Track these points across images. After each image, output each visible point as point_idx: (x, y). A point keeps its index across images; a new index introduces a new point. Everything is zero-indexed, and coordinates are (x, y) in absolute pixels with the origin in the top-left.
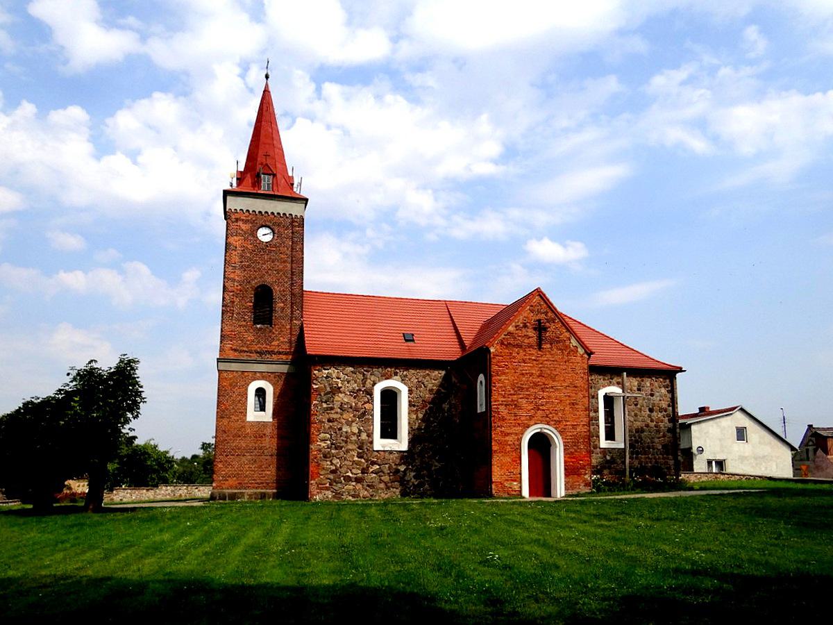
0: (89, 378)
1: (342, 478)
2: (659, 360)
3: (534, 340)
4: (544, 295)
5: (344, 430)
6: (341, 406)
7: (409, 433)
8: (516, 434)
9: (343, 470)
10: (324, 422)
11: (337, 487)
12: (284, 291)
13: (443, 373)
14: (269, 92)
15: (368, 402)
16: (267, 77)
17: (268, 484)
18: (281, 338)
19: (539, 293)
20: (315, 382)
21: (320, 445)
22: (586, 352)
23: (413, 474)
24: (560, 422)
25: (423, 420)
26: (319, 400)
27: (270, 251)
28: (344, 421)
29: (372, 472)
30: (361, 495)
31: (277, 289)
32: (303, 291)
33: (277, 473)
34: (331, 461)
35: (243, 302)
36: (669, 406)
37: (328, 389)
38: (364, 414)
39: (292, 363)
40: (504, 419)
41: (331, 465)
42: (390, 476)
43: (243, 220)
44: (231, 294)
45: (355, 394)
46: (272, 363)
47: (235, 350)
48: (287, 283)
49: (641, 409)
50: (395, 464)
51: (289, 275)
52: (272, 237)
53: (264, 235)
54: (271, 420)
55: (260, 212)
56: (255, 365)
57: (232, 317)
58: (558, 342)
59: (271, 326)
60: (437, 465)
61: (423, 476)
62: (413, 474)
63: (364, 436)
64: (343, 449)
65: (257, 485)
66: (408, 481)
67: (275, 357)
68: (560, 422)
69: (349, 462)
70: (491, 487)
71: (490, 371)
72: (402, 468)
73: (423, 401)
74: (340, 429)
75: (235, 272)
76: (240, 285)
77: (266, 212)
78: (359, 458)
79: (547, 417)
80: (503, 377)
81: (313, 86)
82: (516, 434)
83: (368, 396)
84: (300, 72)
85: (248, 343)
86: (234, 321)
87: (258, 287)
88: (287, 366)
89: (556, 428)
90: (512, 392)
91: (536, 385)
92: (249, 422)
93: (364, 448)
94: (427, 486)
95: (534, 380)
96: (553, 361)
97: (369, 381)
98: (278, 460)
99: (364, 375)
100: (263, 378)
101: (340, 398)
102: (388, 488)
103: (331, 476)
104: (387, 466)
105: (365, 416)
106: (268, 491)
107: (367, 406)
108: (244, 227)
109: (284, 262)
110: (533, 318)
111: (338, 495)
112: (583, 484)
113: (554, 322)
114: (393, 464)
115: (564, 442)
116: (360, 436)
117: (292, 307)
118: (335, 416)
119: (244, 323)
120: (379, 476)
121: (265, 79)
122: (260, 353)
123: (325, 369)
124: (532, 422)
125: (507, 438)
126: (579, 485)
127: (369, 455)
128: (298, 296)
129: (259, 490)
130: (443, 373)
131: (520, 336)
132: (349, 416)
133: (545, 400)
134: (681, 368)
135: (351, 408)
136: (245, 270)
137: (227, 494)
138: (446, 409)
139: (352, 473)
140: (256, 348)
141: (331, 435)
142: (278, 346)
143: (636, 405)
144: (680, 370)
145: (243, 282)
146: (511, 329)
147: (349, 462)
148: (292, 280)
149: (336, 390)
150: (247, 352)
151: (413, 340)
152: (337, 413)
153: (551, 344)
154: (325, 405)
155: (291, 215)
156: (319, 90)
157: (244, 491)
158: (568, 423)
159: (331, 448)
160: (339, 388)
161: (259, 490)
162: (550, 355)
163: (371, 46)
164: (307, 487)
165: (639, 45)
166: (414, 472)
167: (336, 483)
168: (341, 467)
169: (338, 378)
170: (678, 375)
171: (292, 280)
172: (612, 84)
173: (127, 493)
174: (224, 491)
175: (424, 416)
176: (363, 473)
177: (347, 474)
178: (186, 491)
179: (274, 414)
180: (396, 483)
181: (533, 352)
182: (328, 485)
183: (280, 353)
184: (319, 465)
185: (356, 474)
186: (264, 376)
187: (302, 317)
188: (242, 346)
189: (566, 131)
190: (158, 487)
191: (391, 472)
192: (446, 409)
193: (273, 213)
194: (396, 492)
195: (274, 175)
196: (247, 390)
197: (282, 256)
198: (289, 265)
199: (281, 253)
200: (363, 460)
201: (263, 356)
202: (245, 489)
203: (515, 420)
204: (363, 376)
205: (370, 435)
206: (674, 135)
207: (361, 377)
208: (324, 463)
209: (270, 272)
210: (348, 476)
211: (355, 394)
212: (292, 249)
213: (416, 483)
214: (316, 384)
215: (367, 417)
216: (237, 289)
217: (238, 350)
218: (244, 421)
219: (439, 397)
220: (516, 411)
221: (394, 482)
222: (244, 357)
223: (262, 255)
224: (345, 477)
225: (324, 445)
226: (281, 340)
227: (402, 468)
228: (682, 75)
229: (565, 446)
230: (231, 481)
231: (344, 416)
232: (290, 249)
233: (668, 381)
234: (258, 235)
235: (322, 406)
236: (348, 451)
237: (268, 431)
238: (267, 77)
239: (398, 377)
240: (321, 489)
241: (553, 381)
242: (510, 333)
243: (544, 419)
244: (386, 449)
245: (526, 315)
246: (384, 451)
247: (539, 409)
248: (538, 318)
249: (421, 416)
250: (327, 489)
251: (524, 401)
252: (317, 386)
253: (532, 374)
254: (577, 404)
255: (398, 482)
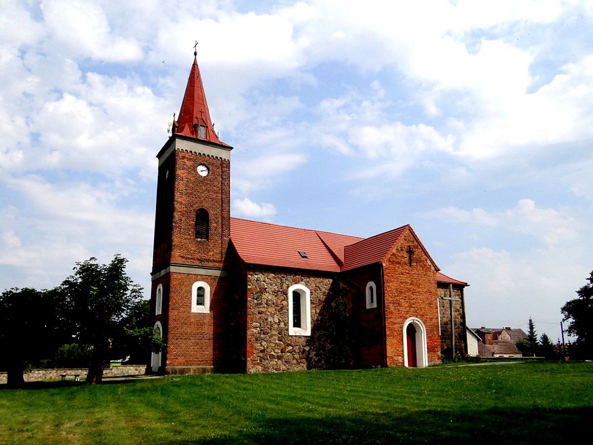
0: (88, 271)
1: (268, 356)
2: (452, 278)
3: (407, 260)
4: (412, 230)
5: (269, 320)
6: (267, 302)
7: (311, 323)
8: (399, 323)
9: (269, 350)
10: (255, 314)
11: (265, 363)
12: (216, 214)
13: (331, 280)
14: (197, 65)
15: (284, 300)
16: (195, 54)
17: (207, 361)
18: (215, 250)
19: (408, 228)
20: (249, 283)
21: (253, 331)
22: (435, 269)
23: (314, 353)
24: (423, 315)
25: (319, 314)
26: (252, 297)
27: (207, 184)
28: (269, 313)
29: (288, 352)
30: (281, 369)
31: (211, 212)
32: (230, 218)
33: (213, 353)
34: (261, 343)
35: (188, 220)
36: (460, 308)
37: (258, 289)
38: (282, 308)
39: (224, 269)
40: (392, 313)
41: (261, 346)
42: (299, 354)
43: (187, 158)
44: (179, 213)
45: (275, 293)
46: (210, 268)
47: (183, 257)
48: (219, 208)
49: (446, 309)
50: (303, 346)
51: (220, 203)
52: (207, 173)
53: (202, 171)
54: (209, 312)
55: (199, 154)
56: (198, 269)
57: (180, 231)
58: (421, 262)
59: (208, 240)
60: (329, 346)
61: (320, 355)
62: (314, 353)
63: (282, 325)
64: (269, 334)
65: (199, 363)
66: (311, 358)
67: (211, 264)
68: (423, 315)
69: (272, 345)
70: (386, 360)
71: (383, 279)
72: (307, 349)
73: (319, 300)
74: (266, 319)
75: (182, 197)
76: (186, 207)
77: (204, 154)
78: (279, 341)
79: (416, 312)
80: (391, 284)
81: (80, 74)
82: (399, 323)
83: (285, 296)
84: (70, 61)
85: (192, 252)
86: (182, 235)
87: (199, 210)
88: (220, 271)
89: (422, 320)
90: (396, 294)
91: (409, 290)
92: (193, 313)
93: (283, 333)
94: (323, 362)
95: (408, 286)
96: (418, 274)
97: (285, 284)
98: (214, 343)
99: (281, 280)
100: (203, 280)
101: (266, 296)
102: (299, 363)
103: (261, 355)
104: (298, 347)
105: (282, 309)
106: (207, 367)
107: (284, 303)
108: (188, 163)
109: (217, 193)
110: (406, 244)
111: (265, 368)
112: (437, 358)
113: (418, 248)
114: (301, 346)
115: (426, 330)
116: (279, 325)
117: (222, 227)
118: (263, 310)
119: (189, 237)
120: (293, 355)
121: (194, 56)
122: (200, 260)
123: (255, 275)
124: (408, 316)
125: (394, 326)
126: (435, 359)
127: (286, 339)
128: (226, 219)
129: (201, 366)
130: (331, 280)
131: (399, 256)
132: (272, 310)
133: (414, 301)
134: (467, 284)
135: (273, 303)
136: (189, 197)
137: (177, 370)
138: (334, 307)
139: (274, 352)
140: (198, 256)
141: (260, 323)
142: (213, 256)
143: (443, 307)
144: (466, 285)
145: (188, 205)
146: (394, 251)
147: (272, 345)
148: (222, 207)
149: (263, 290)
150: (191, 259)
151: (306, 257)
152: (264, 307)
153: (416, 263)
154: (256, 301)
155: (221, 158)
156: (84, 78)
157: (190, 367)
158: (428, 317)
159: (260, 333)
160: (266, 289)
161: (201, 366)
162: (416, 270)
163: (127, 51)
164: (245, 362)
165: (312, 80)
166: (315, 351)
167: (265, 360)
168: (267, 348)
169: (264, 282)
170: (465, 289)
171: (222, 207)
172: (294, 103)
173: (4, 377)
174: (175, 367)
175: (320, 311)
176: (282, 352)
177: (271, 353)
178: (55, 374)
179: (211, 308)
180: (303, 359)
181: (407, 267)
182: (258, 361)
183: (215, 261)
184: (252, 346)
185: (278, 353)
186: (203, 278)
187: (229, 235)
188: (187, 254)
189: (265, 128)
190: (31, 371)
191: (300, 352)
192: (334, 307)
193: (208, 156)
194: (304, 366)
195: (207, 127)
196: (191, 288)
197: (215, 188)
198: (220, 195)
199: (214, 186)
200: (282, 343)
201: (202, 263)
202: (190, 365)
203: (398, 314)
204: (281, 281)
205: (286, 324)
206: (329, 141)
207: (279, 281)
208: (256, 345)
209: (206, 199)
210: (273, 354)
211: (275, 293)
212: (222, 183)
213: (316, 360)
214: (250, 285)
215: (284, 311)
216: (184, 210)
217: (184, 257)
218: (189, 312)
219: (331, 297)
220: (399, 307)
221: (302, 359)
222: (189, 262)
223: (201, 186)
224: (270, 355)
225: (256, 331)
226: (216, 252)
227: (307, 349)
228: (338, 103)
229: (427, 332)
230: (181, 360)
231: (269, 310)
232: (220, 184)
233: (459, 291)
234: (198, 171)
235: (254, 302)
236: (272, 336)
237: (207, 321)
238: (195, 54)
239: (303, 283)
240: (255, 364)
241: (419, 288)
242: (394, 254)
243: (415, 313)
244: (297, 335)
245: (402, 242)
246: (295, 336)
247: (411, 307)
248: (408, 245)
249: (318, 311)
250: (258, 364)
251: (403, 301)
252: (250, 287)
253: (407, 283)
254: (432, 304)
255: (305, 358)
